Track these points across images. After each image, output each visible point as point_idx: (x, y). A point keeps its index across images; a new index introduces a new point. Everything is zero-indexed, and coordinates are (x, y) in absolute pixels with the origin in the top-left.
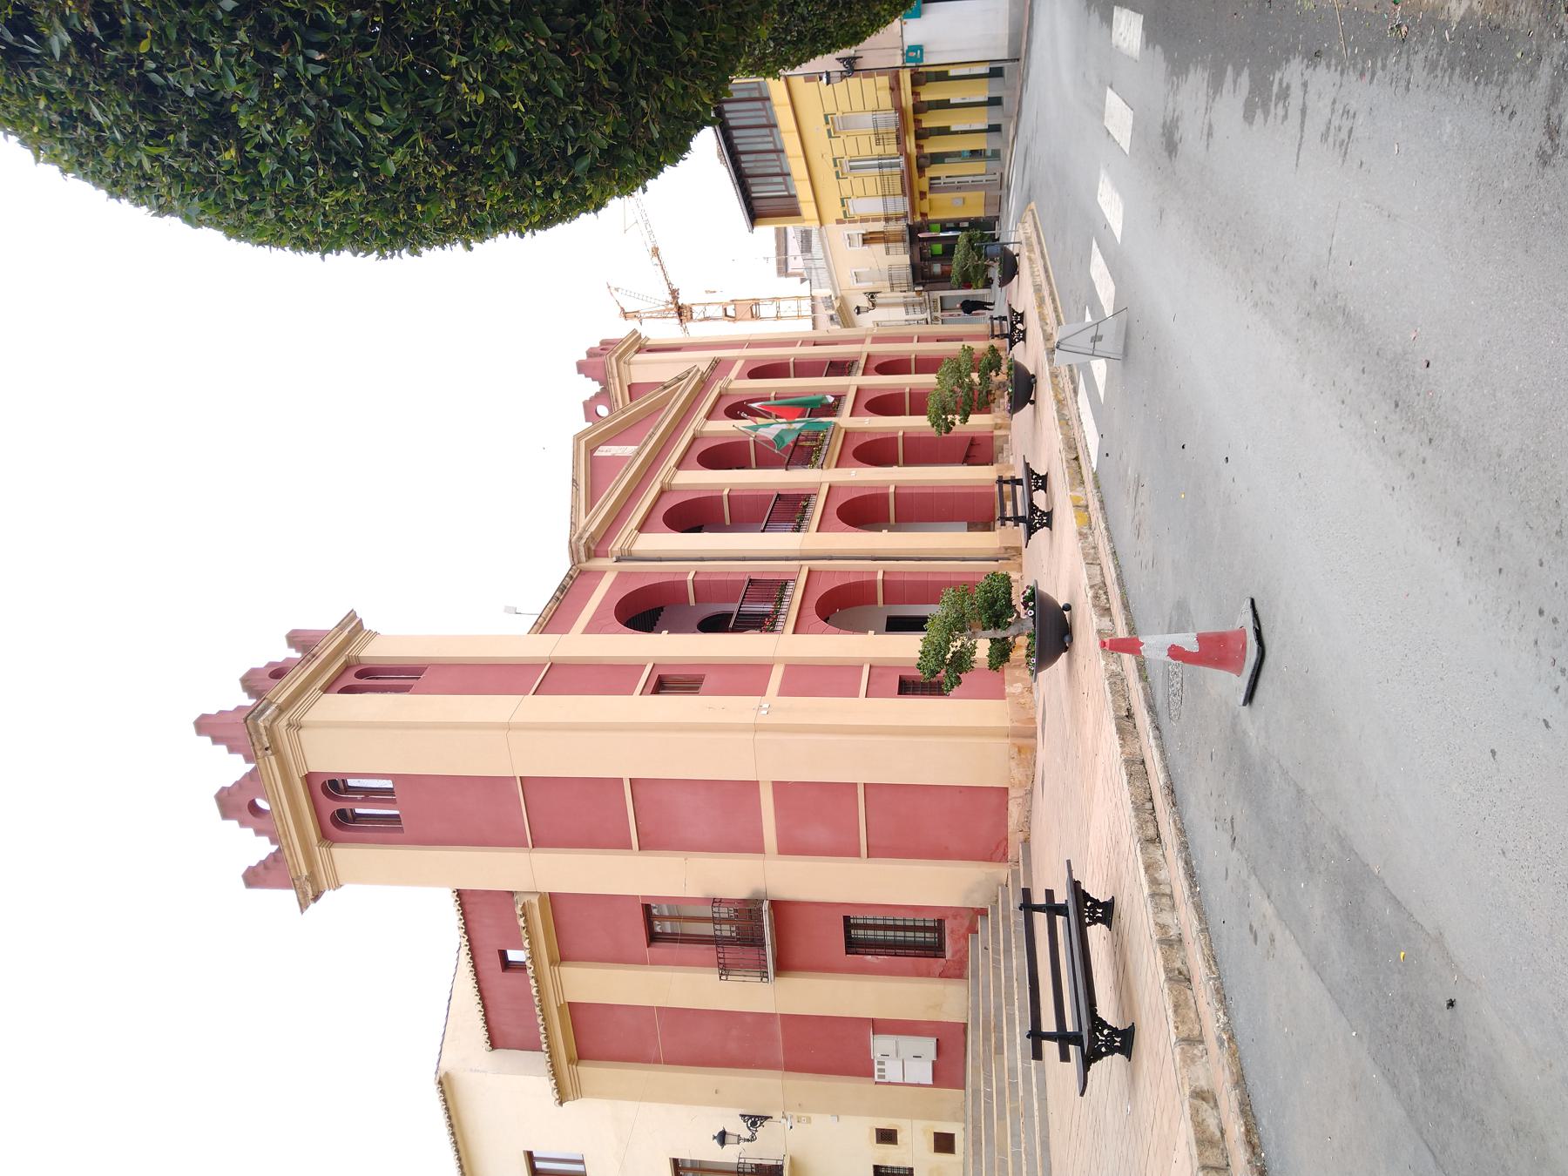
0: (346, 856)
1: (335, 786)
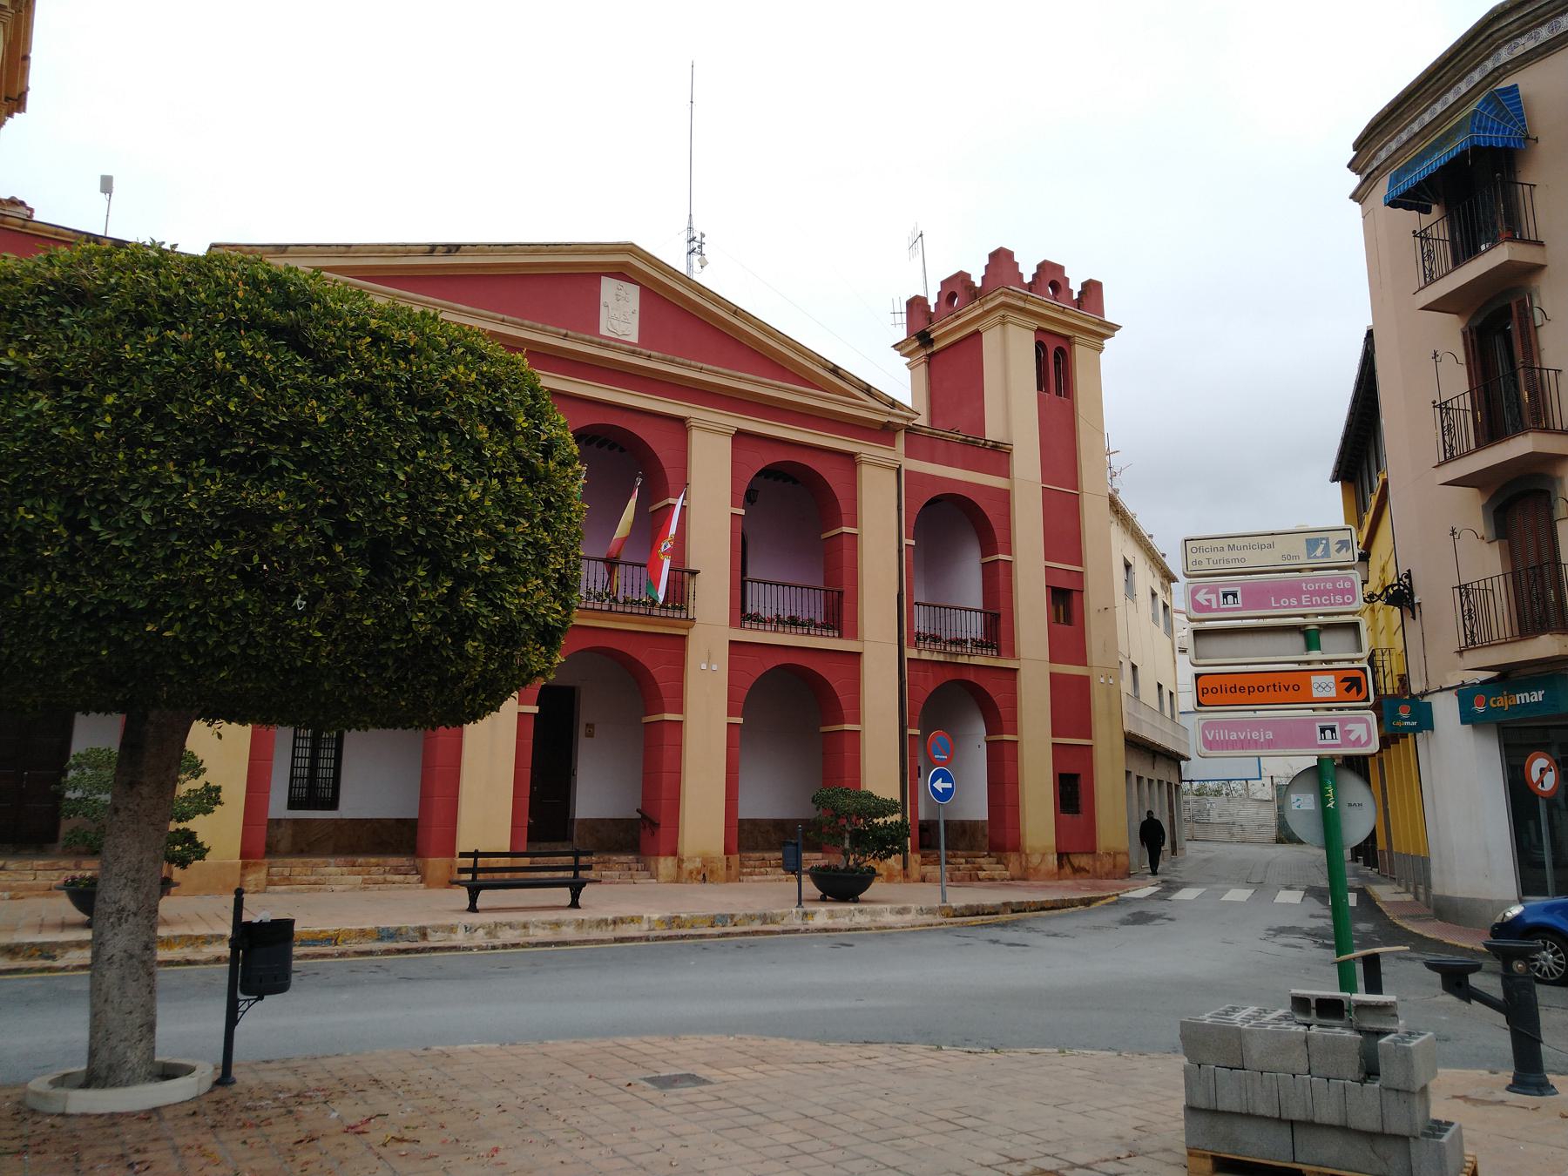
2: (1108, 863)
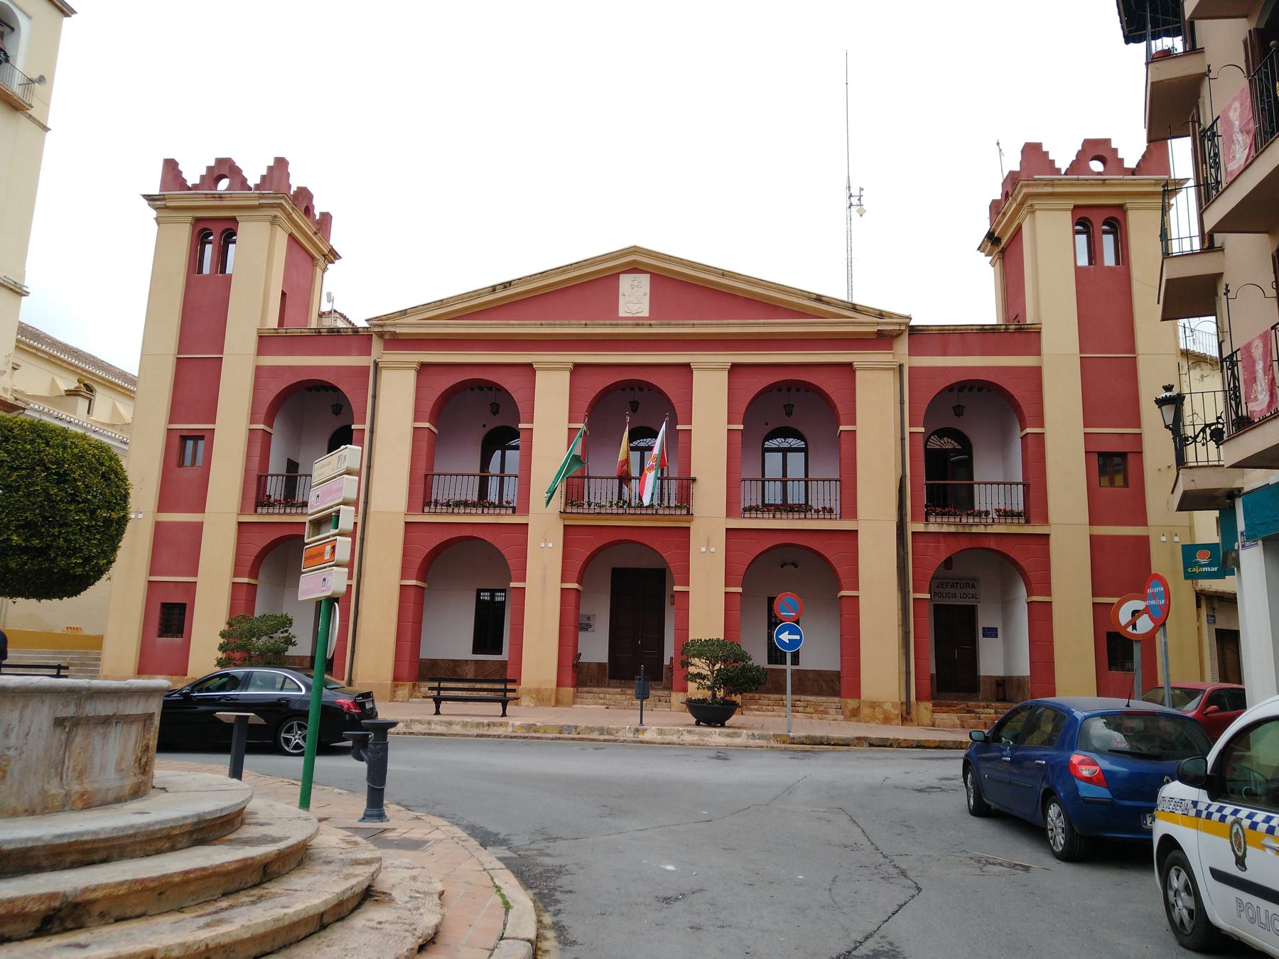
0: (183, 233)
1: (229, 236)
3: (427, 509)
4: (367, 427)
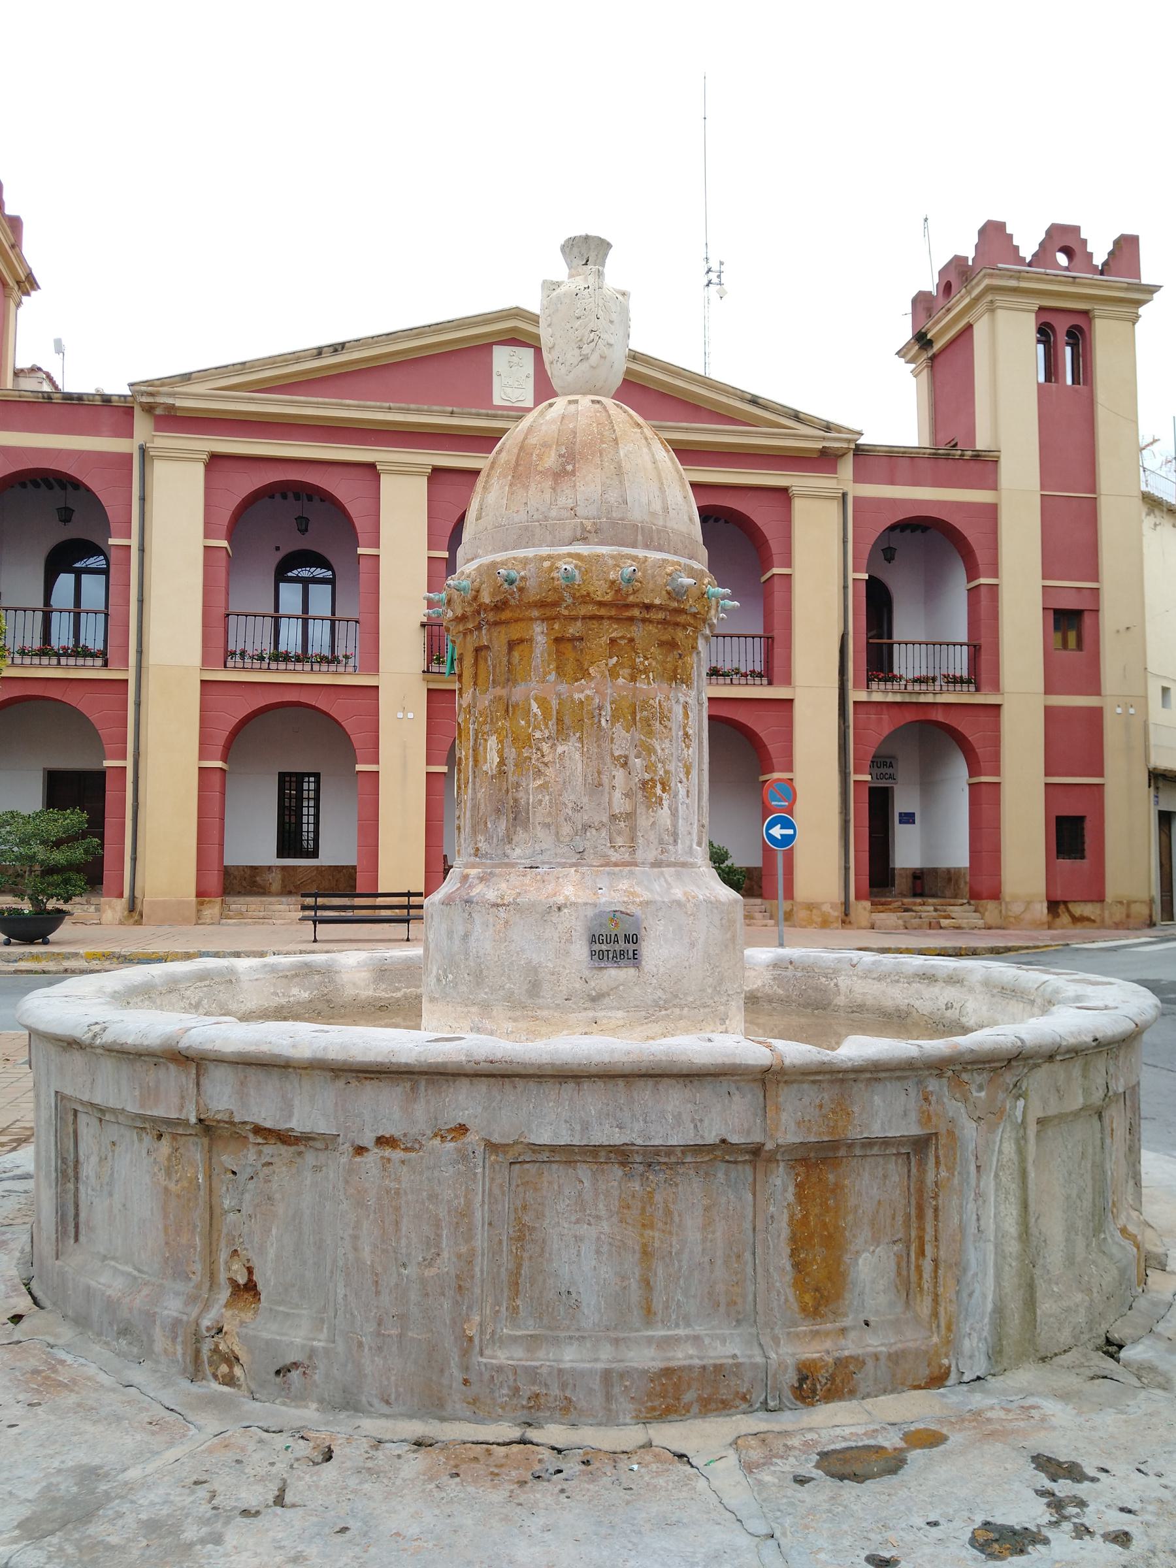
2: (1119, 913)
3: (230, 663)
4: (134, 542)
